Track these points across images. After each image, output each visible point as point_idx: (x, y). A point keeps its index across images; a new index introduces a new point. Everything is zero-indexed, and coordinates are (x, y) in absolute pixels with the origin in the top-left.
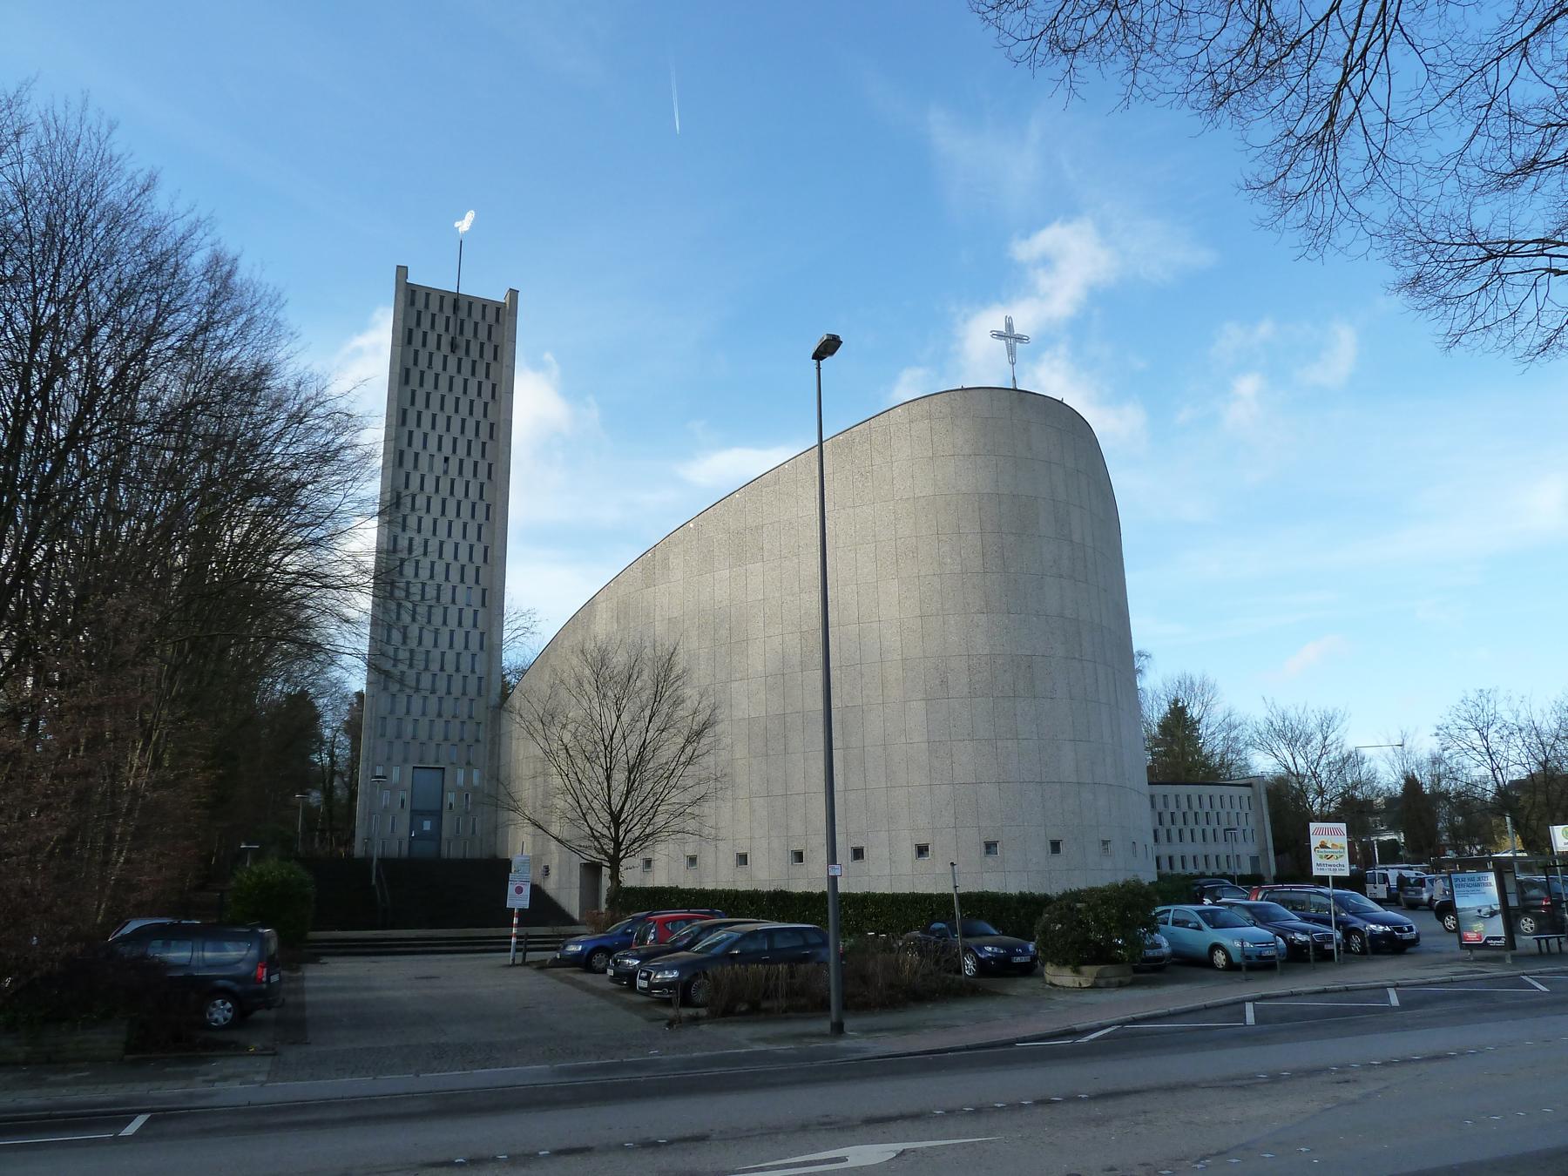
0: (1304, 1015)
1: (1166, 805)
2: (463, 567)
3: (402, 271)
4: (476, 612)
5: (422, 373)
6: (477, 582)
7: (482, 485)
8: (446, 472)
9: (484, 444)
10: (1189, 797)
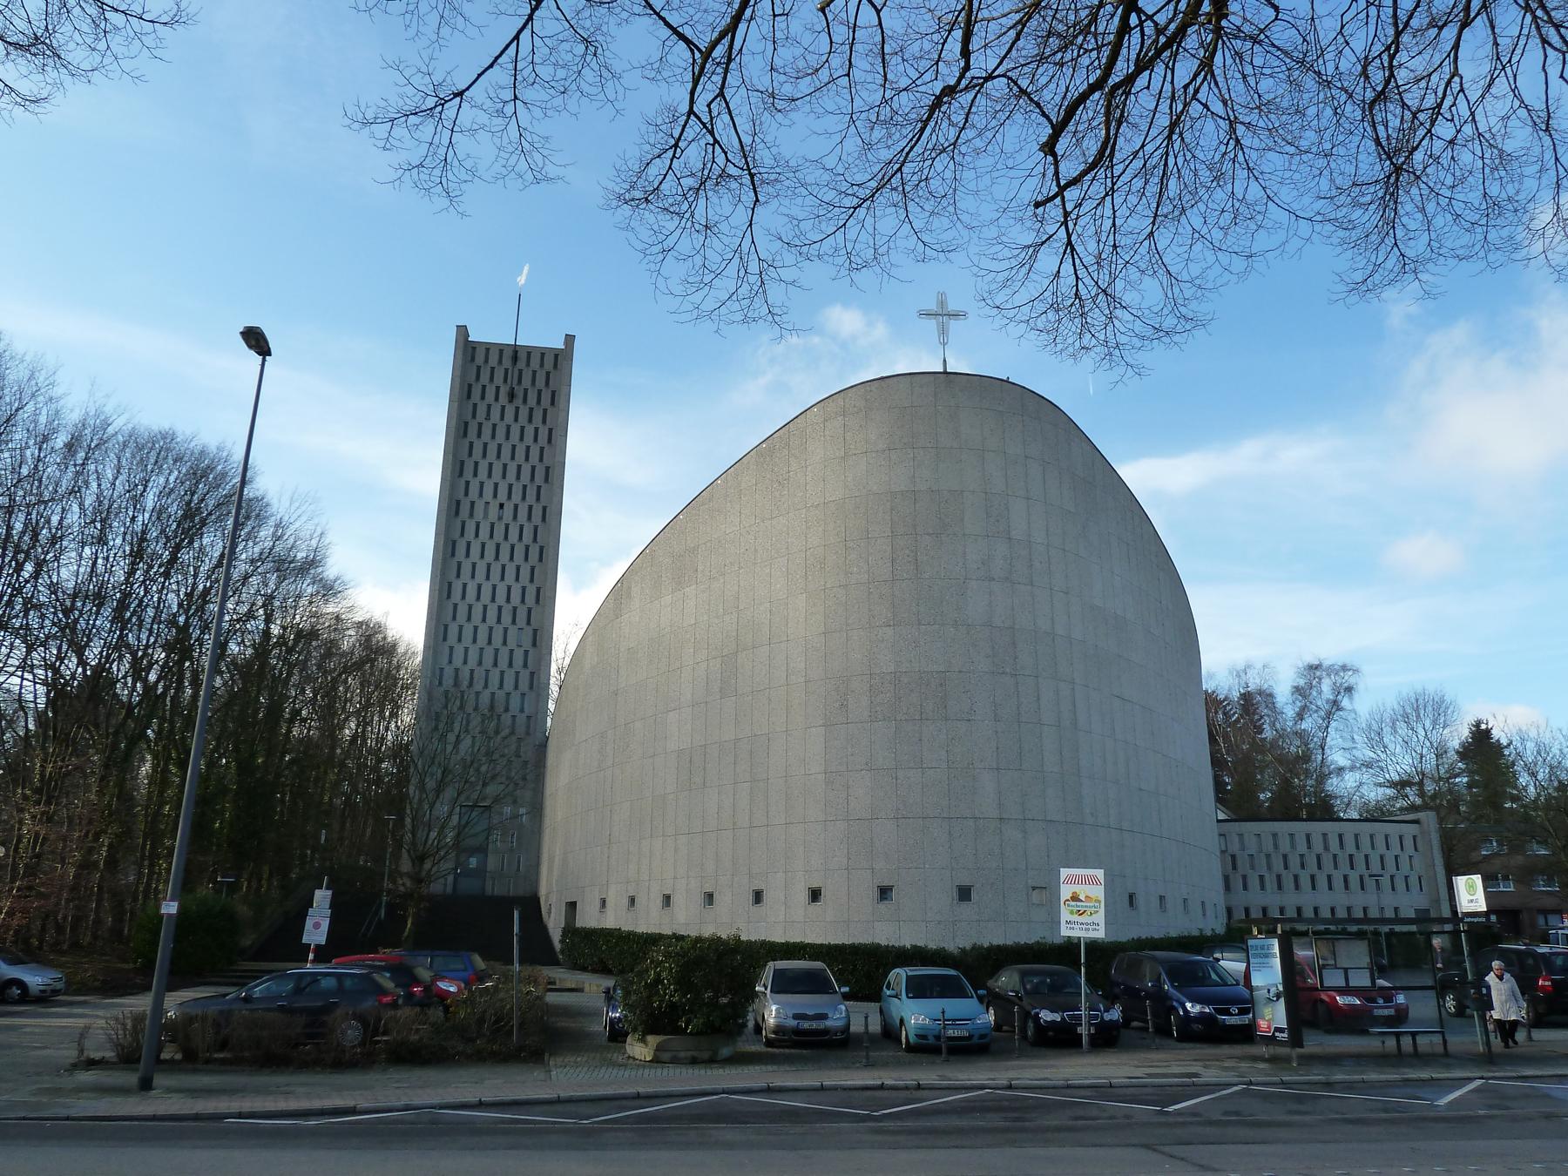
0: (794, 1115)
1: (1293, 846)
2: (515, 609)
3: (462, 331)
4: (526, 652)
5: (480, 425)
6: (529, 623)
7: (536, 528)
8: (500, 518)
9: (539, 488)
10: (1308, 836)
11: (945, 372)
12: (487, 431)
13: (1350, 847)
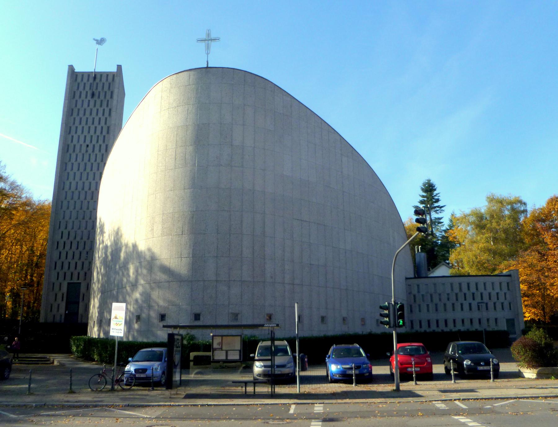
3: (71, 69)
11: (207, 67)
12: (82, 112)
13: (473, 289)
